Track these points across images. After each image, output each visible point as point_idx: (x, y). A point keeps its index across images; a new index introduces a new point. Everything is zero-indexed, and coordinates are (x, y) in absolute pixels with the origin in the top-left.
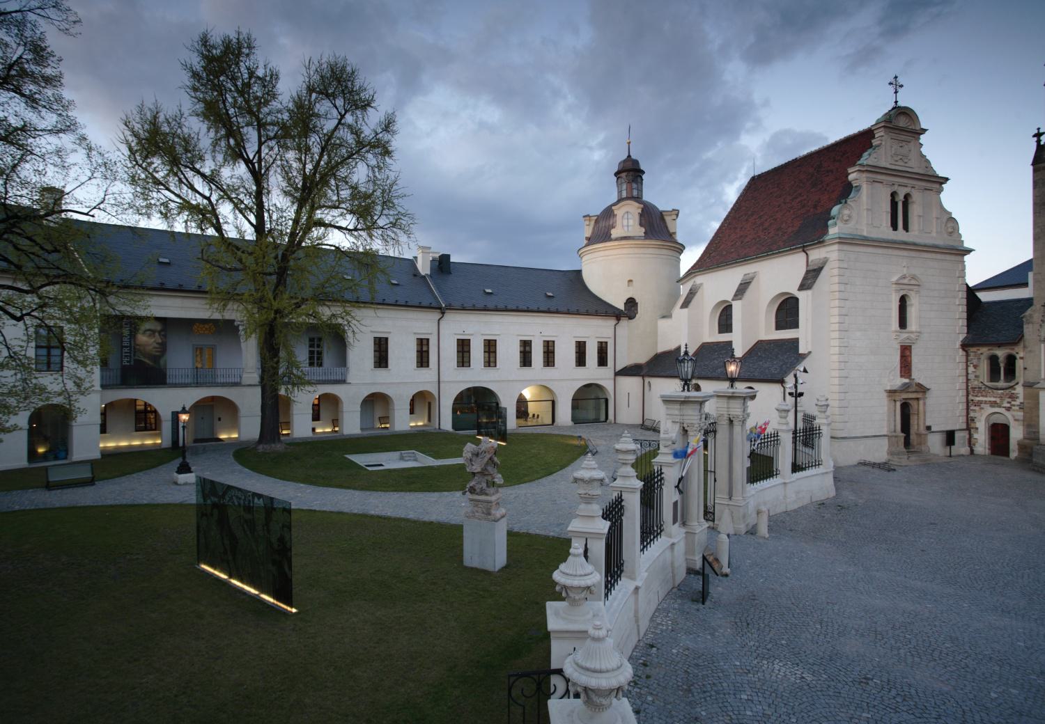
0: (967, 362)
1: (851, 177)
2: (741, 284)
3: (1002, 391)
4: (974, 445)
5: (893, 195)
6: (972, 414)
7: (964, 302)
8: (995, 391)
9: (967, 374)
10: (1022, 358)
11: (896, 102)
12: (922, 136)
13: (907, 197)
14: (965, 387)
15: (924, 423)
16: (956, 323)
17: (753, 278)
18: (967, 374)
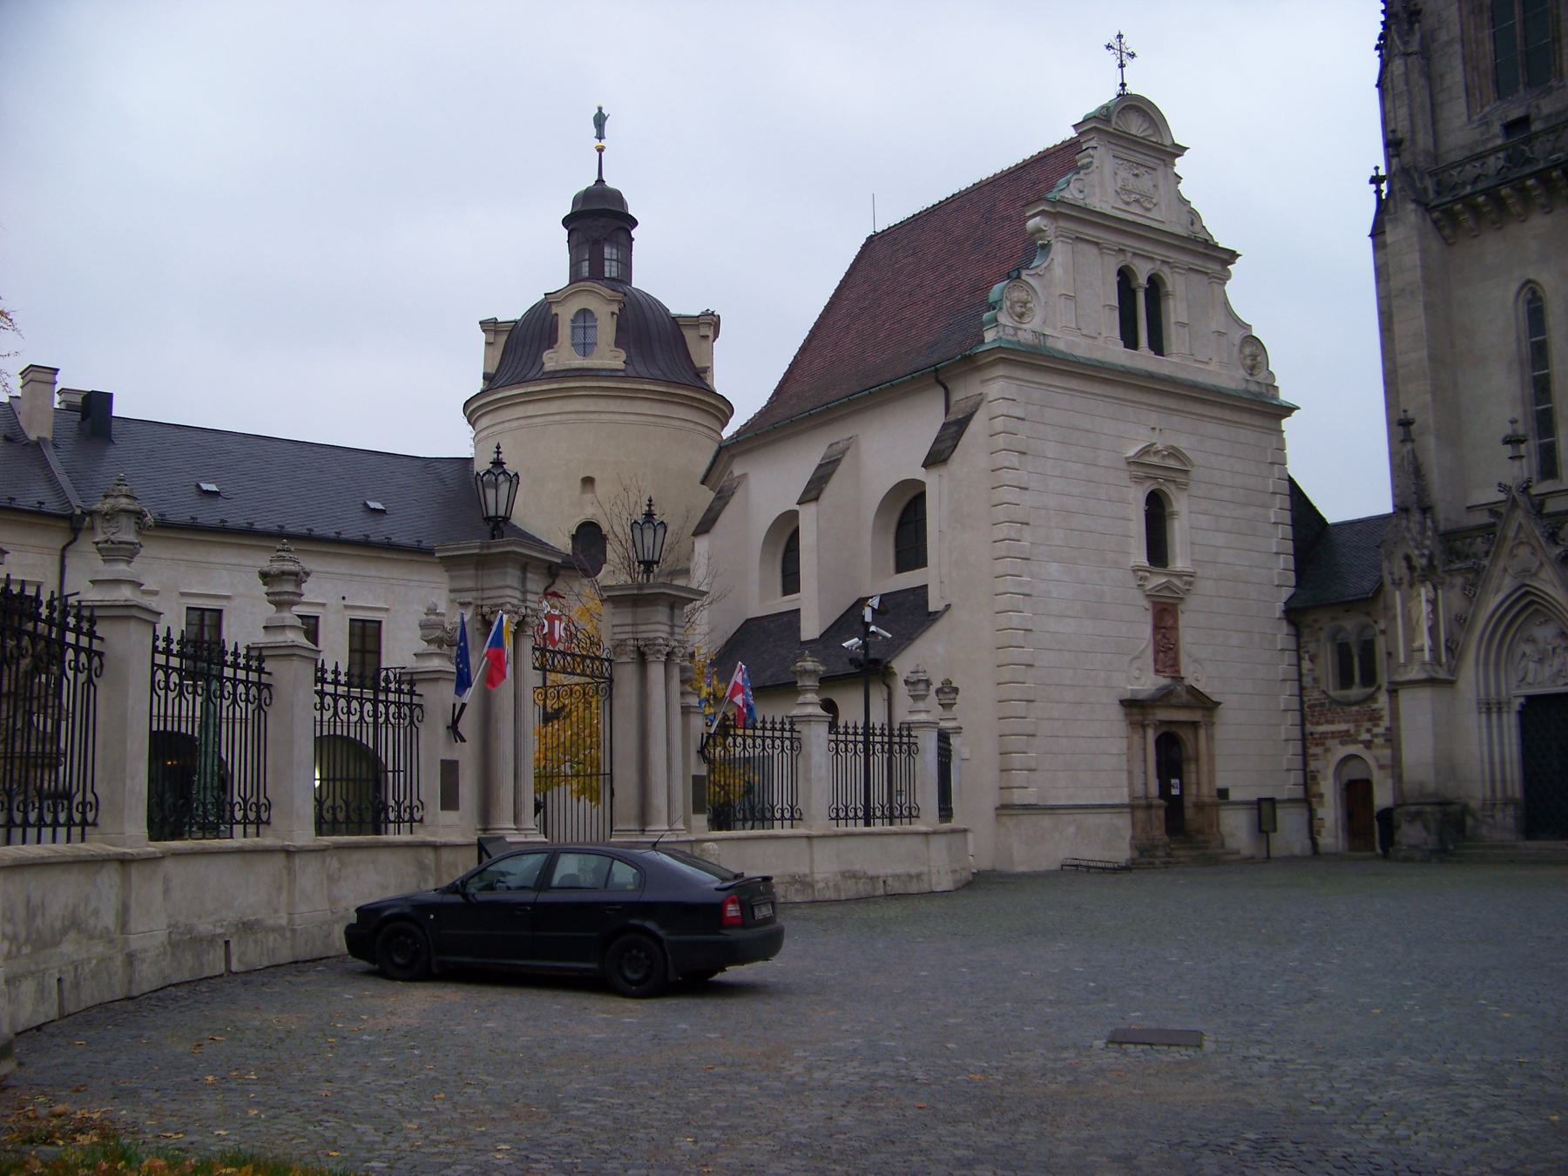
0: (1298, 650)
1: (1031, 224)
2: (820, 466)
3: (1356, 708)
4: (1319, 833)
5: (1125, 276)
6: (1313, 765)
7: (1287, 517)
8: (1347, 709)
9: (1300, 675)
10: (1383, 632)
11: (1123, 85)
12: (1177, 161)
13: (1155, 283)
14: (1297, 707)
15: (1211, 780)
16: (1270, 566)
17: (844, 452)
18: (1300, 675)
